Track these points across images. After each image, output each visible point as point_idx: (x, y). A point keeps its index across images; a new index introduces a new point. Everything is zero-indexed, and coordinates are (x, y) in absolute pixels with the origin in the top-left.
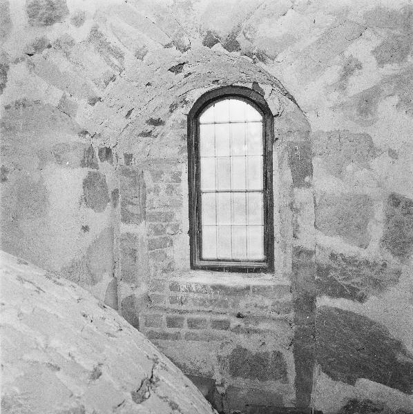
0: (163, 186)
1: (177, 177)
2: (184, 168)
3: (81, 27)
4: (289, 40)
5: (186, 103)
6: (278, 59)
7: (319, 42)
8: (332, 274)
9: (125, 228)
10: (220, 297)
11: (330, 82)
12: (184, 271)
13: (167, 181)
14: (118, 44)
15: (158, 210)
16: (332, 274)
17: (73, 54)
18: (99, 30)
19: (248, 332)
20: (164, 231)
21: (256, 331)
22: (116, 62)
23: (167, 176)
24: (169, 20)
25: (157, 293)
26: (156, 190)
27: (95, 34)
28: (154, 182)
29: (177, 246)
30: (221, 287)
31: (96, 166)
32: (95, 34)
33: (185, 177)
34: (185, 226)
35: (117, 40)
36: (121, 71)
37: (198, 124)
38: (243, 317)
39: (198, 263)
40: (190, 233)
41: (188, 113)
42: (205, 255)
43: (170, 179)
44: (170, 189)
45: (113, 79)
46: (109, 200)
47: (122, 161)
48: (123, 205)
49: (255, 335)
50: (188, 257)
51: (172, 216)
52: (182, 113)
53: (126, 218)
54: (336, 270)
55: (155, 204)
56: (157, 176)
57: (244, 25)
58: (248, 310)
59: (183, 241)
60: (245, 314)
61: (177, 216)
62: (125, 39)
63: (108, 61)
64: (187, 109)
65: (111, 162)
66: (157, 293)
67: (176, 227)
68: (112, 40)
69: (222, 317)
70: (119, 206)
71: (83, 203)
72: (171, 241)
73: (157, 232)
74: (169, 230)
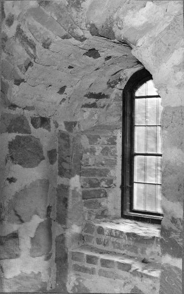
0: (98, 149)
1: (112, 141)
2: (119, 134)
3: (12, 27)
4: (148, 27)
5: (120, 80)
6: (139, 44)
7: (168, 28)
8: (173, 235)
9: (61, 180)
10: (132, 243)
11: (177, 62)
12: (116, 218)
13: (103, 144)
14: (32, 38)
15: (93, 167)
16: (173, 235)
17: (7, 47)
18: (21, 28)
19: (142, 276)
20: (98, 184)
21: (148, 276)
22: (32, 51)
23: (103, 140)
24: (66, 17)
25: (89, 234)
26: (93, 151)
27: (19, 32)
28: (90, 144)
29: (111, 196)
30: (134, 235)
31: (27, 131)
32: (19, 32)
33: (119, 140)
34: (118, 181)
35: (31, 35)
36: (35, 58)
37: (133, 98)
38: (146, 263)
39: (128, 212)
40: (123, 187)
41: (123, 88)
42: (135, 207)
43: (106, 142)
44: (105, 151)
45: (30, 64)
46: (43, 158)
47: (63, 128)
48: (60, 163)
49: (147, 279)
50: (119, 207)
51: (107, 171)
52: (117, 91)
53: (62, 172)
54: (176, 232)
55: (91, 162)
56: (93, 139)
57: (115, 17)
58: (152, 257)
59: (115, 194)
60: (150, 260)
61: (112, 173)
62: (37, 34)
63: (28, 52)
64: (122, 85)
65: (49, 128)
66: (89, 234)
67: (111, 181)
68: (29, 35)
69: (127, 261)
70: (56, 163)
71: (9, 161)
72: (106, 193)
73: (92, 185)
74: (103, 184)
